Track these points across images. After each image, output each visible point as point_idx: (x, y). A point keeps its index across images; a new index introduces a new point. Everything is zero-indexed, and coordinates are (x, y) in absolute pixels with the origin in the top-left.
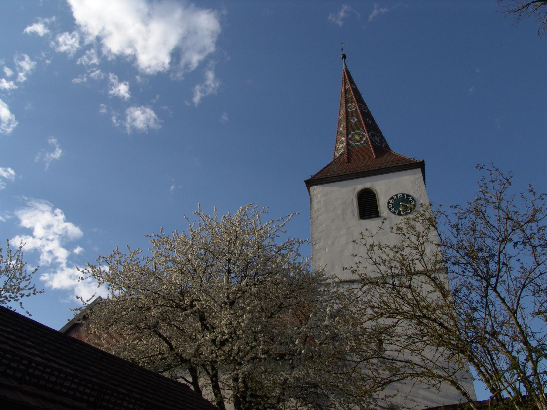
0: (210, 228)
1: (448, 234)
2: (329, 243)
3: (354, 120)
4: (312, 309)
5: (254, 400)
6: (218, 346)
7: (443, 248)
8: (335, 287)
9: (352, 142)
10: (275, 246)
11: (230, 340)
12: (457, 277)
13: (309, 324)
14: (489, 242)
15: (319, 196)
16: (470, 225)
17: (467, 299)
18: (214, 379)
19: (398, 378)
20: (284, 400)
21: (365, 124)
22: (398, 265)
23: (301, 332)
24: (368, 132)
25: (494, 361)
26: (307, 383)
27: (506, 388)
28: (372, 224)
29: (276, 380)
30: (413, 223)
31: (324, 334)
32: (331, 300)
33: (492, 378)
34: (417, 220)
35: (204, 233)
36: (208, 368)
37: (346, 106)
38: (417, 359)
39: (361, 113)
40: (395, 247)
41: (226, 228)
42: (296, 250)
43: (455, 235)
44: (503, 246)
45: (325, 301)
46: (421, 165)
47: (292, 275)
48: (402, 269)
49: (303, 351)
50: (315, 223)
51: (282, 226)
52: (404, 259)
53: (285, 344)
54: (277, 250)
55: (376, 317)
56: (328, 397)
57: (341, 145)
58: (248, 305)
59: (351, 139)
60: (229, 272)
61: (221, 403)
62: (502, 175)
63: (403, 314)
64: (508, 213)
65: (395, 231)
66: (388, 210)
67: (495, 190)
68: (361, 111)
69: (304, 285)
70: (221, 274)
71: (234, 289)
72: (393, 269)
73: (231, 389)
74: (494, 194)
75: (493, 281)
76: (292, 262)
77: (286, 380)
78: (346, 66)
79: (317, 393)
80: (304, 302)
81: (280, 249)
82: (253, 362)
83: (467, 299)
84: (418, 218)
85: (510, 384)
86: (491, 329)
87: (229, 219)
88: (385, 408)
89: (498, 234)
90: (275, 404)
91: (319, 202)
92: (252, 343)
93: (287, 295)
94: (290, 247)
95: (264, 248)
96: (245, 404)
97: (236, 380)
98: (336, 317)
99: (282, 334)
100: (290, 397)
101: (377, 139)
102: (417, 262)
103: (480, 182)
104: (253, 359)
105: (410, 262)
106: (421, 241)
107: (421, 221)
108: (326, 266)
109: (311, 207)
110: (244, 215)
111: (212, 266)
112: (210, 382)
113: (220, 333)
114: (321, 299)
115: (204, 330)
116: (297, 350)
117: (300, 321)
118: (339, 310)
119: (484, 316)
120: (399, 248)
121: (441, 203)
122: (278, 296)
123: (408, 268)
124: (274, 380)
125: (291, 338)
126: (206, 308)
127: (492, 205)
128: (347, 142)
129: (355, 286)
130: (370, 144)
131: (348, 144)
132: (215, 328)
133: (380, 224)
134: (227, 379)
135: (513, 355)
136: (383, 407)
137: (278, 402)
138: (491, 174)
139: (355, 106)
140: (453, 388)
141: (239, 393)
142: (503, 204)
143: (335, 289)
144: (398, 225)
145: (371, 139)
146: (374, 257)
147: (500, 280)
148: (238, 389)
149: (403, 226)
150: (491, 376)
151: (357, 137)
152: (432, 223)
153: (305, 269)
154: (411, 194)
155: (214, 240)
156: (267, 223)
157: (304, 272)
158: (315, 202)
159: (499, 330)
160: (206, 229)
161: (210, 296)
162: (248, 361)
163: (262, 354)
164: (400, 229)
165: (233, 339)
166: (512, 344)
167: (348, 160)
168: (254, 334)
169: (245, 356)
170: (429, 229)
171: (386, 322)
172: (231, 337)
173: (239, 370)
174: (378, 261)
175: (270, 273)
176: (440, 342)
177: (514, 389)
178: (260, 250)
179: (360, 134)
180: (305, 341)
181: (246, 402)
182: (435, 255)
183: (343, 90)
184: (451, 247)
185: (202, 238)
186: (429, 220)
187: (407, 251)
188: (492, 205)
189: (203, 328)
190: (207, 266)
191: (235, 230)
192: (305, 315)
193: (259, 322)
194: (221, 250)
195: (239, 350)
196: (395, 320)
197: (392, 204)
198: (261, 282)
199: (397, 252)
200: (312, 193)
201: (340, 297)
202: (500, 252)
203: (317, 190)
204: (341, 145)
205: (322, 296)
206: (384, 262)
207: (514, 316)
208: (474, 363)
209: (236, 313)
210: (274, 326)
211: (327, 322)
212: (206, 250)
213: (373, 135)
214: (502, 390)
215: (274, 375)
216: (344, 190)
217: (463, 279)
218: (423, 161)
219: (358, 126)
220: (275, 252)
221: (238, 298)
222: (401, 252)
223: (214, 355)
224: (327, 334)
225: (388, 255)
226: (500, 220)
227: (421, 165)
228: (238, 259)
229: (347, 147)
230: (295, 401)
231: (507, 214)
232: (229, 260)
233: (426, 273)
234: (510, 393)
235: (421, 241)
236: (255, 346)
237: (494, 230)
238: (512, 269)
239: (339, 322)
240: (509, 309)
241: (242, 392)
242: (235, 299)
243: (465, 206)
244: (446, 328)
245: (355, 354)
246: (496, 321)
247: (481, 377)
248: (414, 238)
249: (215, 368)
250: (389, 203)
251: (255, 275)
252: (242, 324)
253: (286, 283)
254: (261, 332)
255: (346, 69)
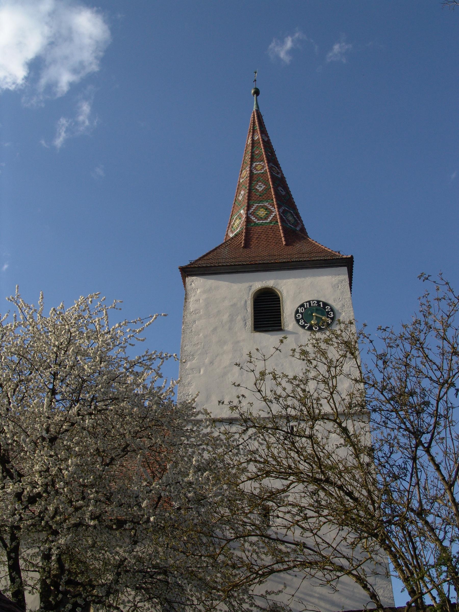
0: (31, 325)
1: (372, 366)
2: (207, 361)
3: (260, 187)
4: (172, 456)
5: (72, 590)
6: (25, 503)
7: (362, 386)
8: (208, 426)
9: (253, 218)
10: (126, 359)
11: (44, 495)
12: (378, 428)
13: (164, 478)
14: (426, 383)
15: (198, 292)
16: (402, 357)
17: (387, 462)
18: (13, 555)
19: (286, 567)
20: (117, 591)
21: (276, 194)
22: (297, 403)
23: (151, 490)
24: (279, 208)
25: (417, 552)
26: (154, 567)
27: (429, 592)
28: (269, 340)
29: (109, 559)
30: (323, 346)
31: (185, 494)
32: (201, 445)
33: (413, 575)
34: (331, 342)
35: (21, 331)
36: (5, 536)
37: (251, 165)
38: (310, 541)
39: (271, 178)
40: (295, 378)
41: (54, 326)
42: (157, 369)
43: (381, 369)
44: (444, 390)
45: (192, 446)
46: (348, 263)
47: (147, 403)
48: (301, 410)
49: (152, 519)
50: (188, 331)
51: (140, 331)
52: (306, 397)
53: (126, 506)
54: (128, 366)
55: (258, 476)
56: (183, 590)
57: (238, 222)
58: (77, 444)
59: (253, 214)
60: (53, 392)
61: (19, 594)
62: (453, 292)
63: (298, 474)
64: (455, 346)
65: (297, 355)
66: (295, 322)
67: (441, 312)
68: (271, 175)
69: (164, 419)
70: (41, 394)
71: (57, 418)
72: (289, 409)
73: (39, 571)
74: (439, 317)
75: (425, 438)
76: (149, 386)
77: (123, 561)
78: (258, 106)
79: (168, 582)
80: (161, 445)
81: (133, 365)
82: (76, 530)
83: (387, 462)
84: (331, 340)
85: (436, 586)
86: (417, 505)
87: (60, 313)
88: (264, 609)
89: (438, 374)
90: (102, 597)
91: (198, 300)
92: (78, 501)
93: (136, 432)
94: (149, 363)
95: (110, 362)
96: (57, 596)
97: (47, 557)
98: (205, 470)
99: (123, 490)
100: (127, 586)
101: (290, 218)
102: (324, 402)
103: (422, 298)
104: (77, 525)
105: (315, 402)
106: (333, 374)
107: (336, 345)
108: (198, 395)
109: (185, 307)
110: (84, 311)
111: (29, 381)
112: (5, 558)
113: (30, 483)
114: (186, 442)
115: (4, 478)
116: (143, 515)
117: (153, 472)
118: (212, 462)
119: (407, 488)
120: (301, 381)
121: (366, 322)
122: (124, 434)
123: (311, 410)
124: (105, 558)
125: (137, 497)
126: (11, 444)
127: (433, 333)
128: (248, 218)
129: (234, 429)
130: (279, 224)
131: (248, 220)
132: (23, 476)
133: (277, 344)
134: (34, 555)
135: (443, 544)
136: (261, 609)
137: (108, 594)
138: (438, 289)
139: (263, 167)
140: (359, 587)
141: (49, 577)
142: (450, 333)
143: (209, 430)
144: (303, 348)
145: (281, 218)
146: (264, 390)
147: (437, 437)
148: (49, 572)
149: (310, 349)
150: (412, 574)
151: (262, 213)
152: (350, 348)
153: (168, 397)
154: (330, 302)
155: (35, 342)
156: (117, 325)
157: (166, 401)
158: (192, 299)
159: (429, 508)
160: (24, 324)
161: (20, 427)
162: (69, 529)
163: (92, 519)
164: (304, 353)
165: (48, 493)
166: (445, 528)
167: (245, 244)
168: (81, 488)
169: (65, 521)
170: (345, 356)
171: (275, 484)
172: (46, 491)
173: (53, 541)
174: (270, 396)
175: (115, 399)
176: (345, 518)
177: (441, 593)
178: (102, 365)
179: (267, 209)
180: (157, 503)
181: (59, 592)
182: (351, 395)
183: (250, 141)
184: (373, 386)
185: (16, 338)
186: (347, 344)
187: (311, 386)
188: (433, 333)
189: (5, 474)
190: (21, 381)
191: (69, 330)
192: (160, 465)
193: (92, 471)
194: (45, 358)
195: (56, 512)
196: (287, 482)
197: (301, 313)
198: (100, 411)
199: (298, 385)
200: (188, 287)
201: (215, 442)
202: (439, 399)
203: (197, 283)
204: (238, 222)
205: (188, 438)
206: (278, 397)
207: (450, 489)
208: (391, 552)
209: (57, 455)
210: (113, 478)
211: (190, 478)
212: (22, 357)
213: (284, 212)
214: (424, 594)
215: (106, 552)
216: (236, 287)
217: (386, 431)
218: (352, 257)
219: (265, 196)
220: (125, 368)
221: (63, 433)
222: (302, 386)
223: (17, 517)
224: (189, 495)
225: (284, 389)
226: (443, 354)
227: (348, 263)
228: (70, 374)
229: (246, 225)
230: (133, 593)
231: (454, 348)
232: (55, 375)
233: (335, 418)
234: (434, 598)
235: (333, 374)
236: (80, 508)
237: (434, 367)
238: (454, 424)
239: (208, 479)
240: (444, 479)
241: (55, 576)
242: (59, 434)
243: (398, 330)
244: (355, 500)
245: (228, 527)
246: (426, 495)
247: (398, 573)
248: (323, 369)
249: (16, 538)
250: (297, 312)
251: (92, 400)
252: (65, 472)
253: (137, 415)
254: (92, 486)
255: (257, 111)
